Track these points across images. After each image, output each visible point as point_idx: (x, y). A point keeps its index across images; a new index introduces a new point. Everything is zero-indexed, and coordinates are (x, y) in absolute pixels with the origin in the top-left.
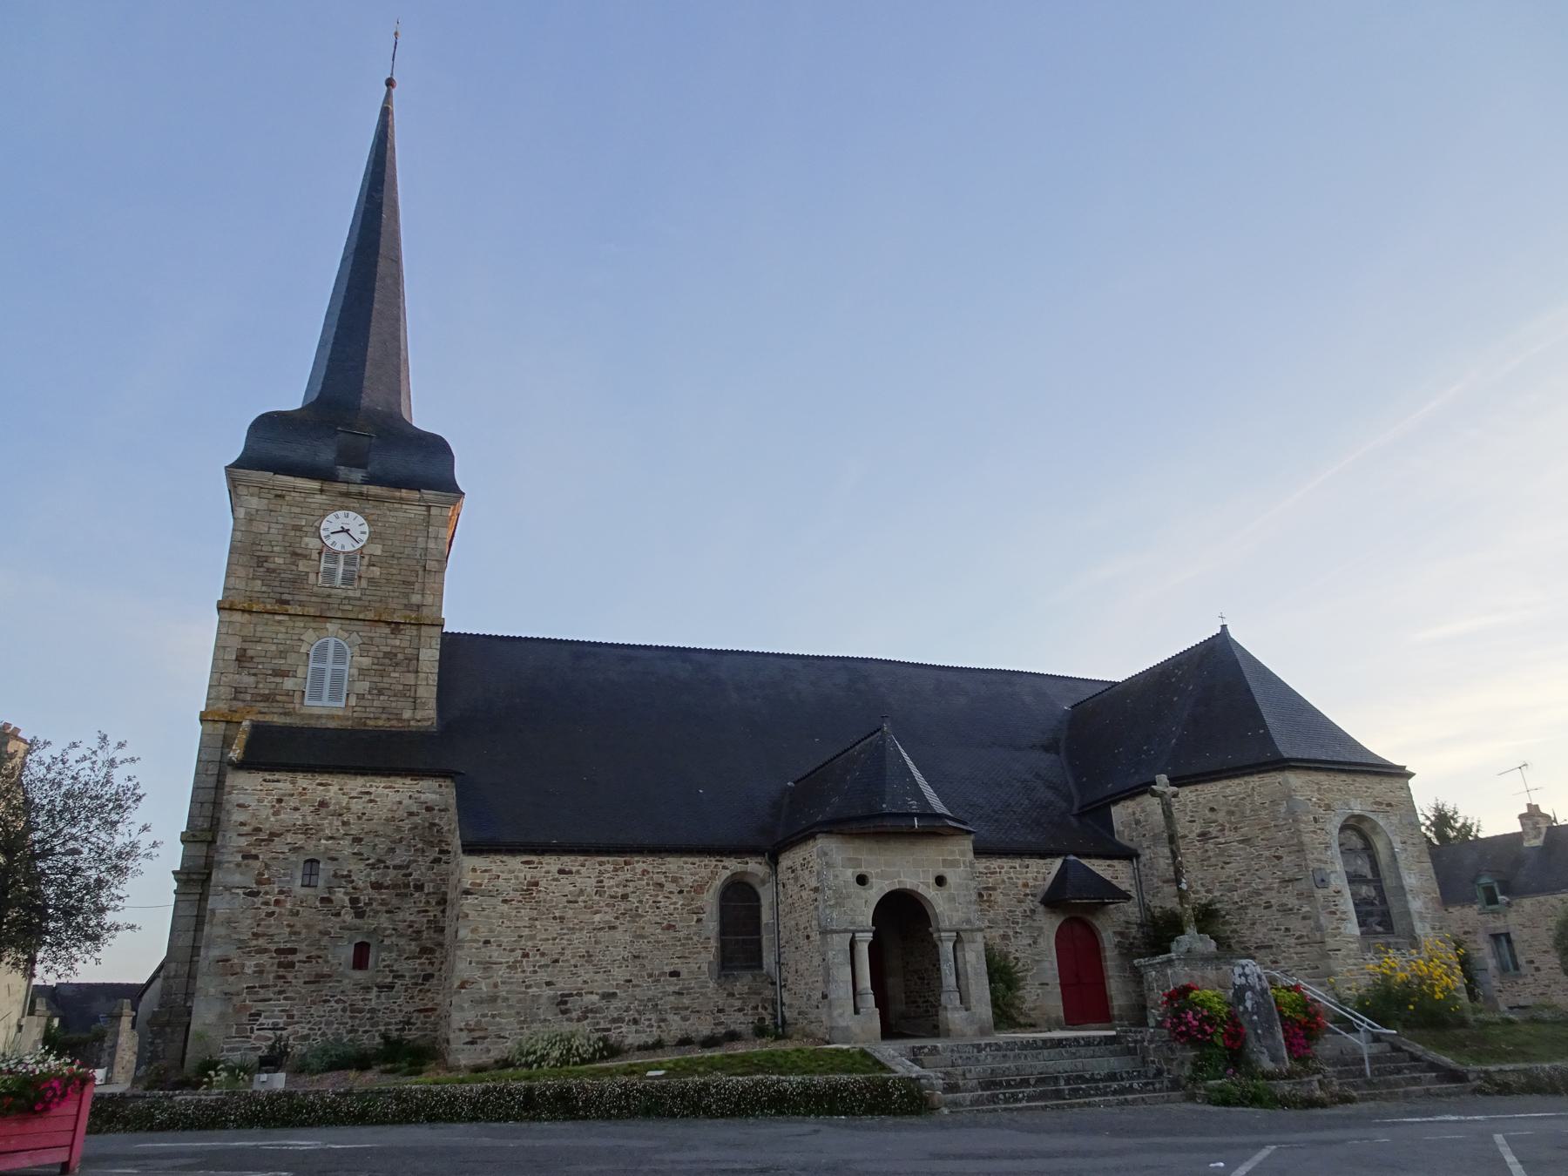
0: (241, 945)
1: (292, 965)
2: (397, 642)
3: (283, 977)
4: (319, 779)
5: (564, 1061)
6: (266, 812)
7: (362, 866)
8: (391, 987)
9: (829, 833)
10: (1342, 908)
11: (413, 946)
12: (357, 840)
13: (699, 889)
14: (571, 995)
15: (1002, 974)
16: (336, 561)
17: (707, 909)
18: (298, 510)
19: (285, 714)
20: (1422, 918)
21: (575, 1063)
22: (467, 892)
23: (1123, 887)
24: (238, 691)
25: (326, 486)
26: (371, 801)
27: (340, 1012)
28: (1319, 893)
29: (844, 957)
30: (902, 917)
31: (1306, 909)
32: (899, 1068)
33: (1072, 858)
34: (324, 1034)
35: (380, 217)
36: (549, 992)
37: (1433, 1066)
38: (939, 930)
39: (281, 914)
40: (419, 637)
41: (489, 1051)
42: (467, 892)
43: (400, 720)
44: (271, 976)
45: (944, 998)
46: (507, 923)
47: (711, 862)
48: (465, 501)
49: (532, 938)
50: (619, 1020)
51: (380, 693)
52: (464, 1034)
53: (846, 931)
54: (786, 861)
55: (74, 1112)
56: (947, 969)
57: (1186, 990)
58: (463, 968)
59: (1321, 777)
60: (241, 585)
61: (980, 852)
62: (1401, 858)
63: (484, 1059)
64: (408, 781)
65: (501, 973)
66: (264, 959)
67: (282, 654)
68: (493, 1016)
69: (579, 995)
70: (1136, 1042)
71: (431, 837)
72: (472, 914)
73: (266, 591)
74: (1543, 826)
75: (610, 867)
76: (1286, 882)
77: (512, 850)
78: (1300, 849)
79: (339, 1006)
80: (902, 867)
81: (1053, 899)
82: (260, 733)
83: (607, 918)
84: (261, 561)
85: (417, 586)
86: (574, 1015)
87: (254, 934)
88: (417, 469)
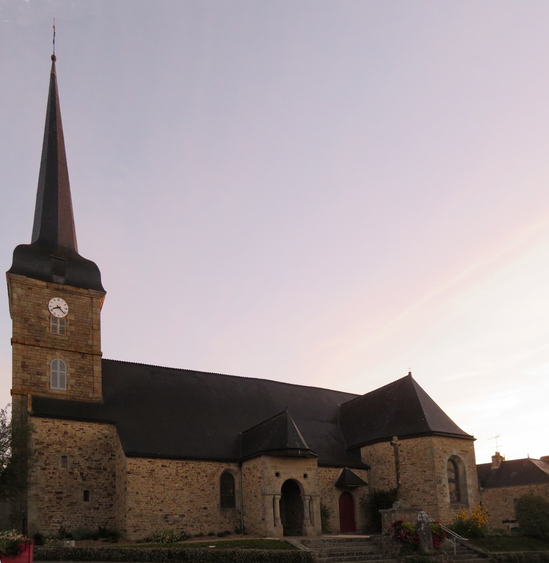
0: (42, 489)
1: (61, 498)
2: (84, 362)
3: (59, 503)
4: (63, 422)
5: (171, 540)
6: (45, 435)
7: (83, 460)
8: (98, 509)
9: (266, 455)
10: (445, 492)
11: (105, 493)
12: (80, 449)
13: (213, 475)
14: (169, 515)
15: (325, 514)
16: (56, 323)
17: (216, 484)
18: (38, 296)
19: (44, 392)
20: (471, 497)
21: (175, 541)
22: (129, 473)
23: (365, 480)
24: (24, 381)
25: (49, 284)
26: (84, 432)
27: (81, 518)
28: (438, 486)
29: (270, 505)
30: (291, 489)
31: (432, 492)
32: (301, 548)
33: (347, 468)
34: (76, 526)
35: (57, 140)
36: (161, 514)
37: (476, 552)
38: (304, 496)
39: (55, 478)
40: (93, 360)
41: (141, 535)
42: (129, 473)
43: (89, 398)
44: (55, 502)
45: (305, 521)
46: (144, 486)
47: (217, 464)
48: (107, 296)
49: (154, 492)
50: (186, 525)
51: (80, 385)
52: (132, 528)
53: (272, 495)
54: (245, 466)
55: (28, 555)
56: (306, 511)
57: (400, 522)
58: (130, 503)
59: (444, 440)
60: (19, 331)
61: (320, 465)
62: (467, 473)
63: (140, 538)
64: (97, 425)
65: (143, 505)
66: (51, 495)
67: (40, 365)
68: (142, 522)
69: (172, 515)
70: (378, 540)
71: (108, 450)
72: (131, 481)
73: (29, 337)
74: (500, 461)
75: (180, 465)
76: (426, 481)
77: (144, 456)
78: (433, 468)
79: (80, 515)
80: (293, 471)
81: (340, 484)
82: (36, 401)
83: (180, 485)
84: (26, 320)
85: (90, 336)
86: (170, 523)
87: (46, 485)
88: (84, 280)
